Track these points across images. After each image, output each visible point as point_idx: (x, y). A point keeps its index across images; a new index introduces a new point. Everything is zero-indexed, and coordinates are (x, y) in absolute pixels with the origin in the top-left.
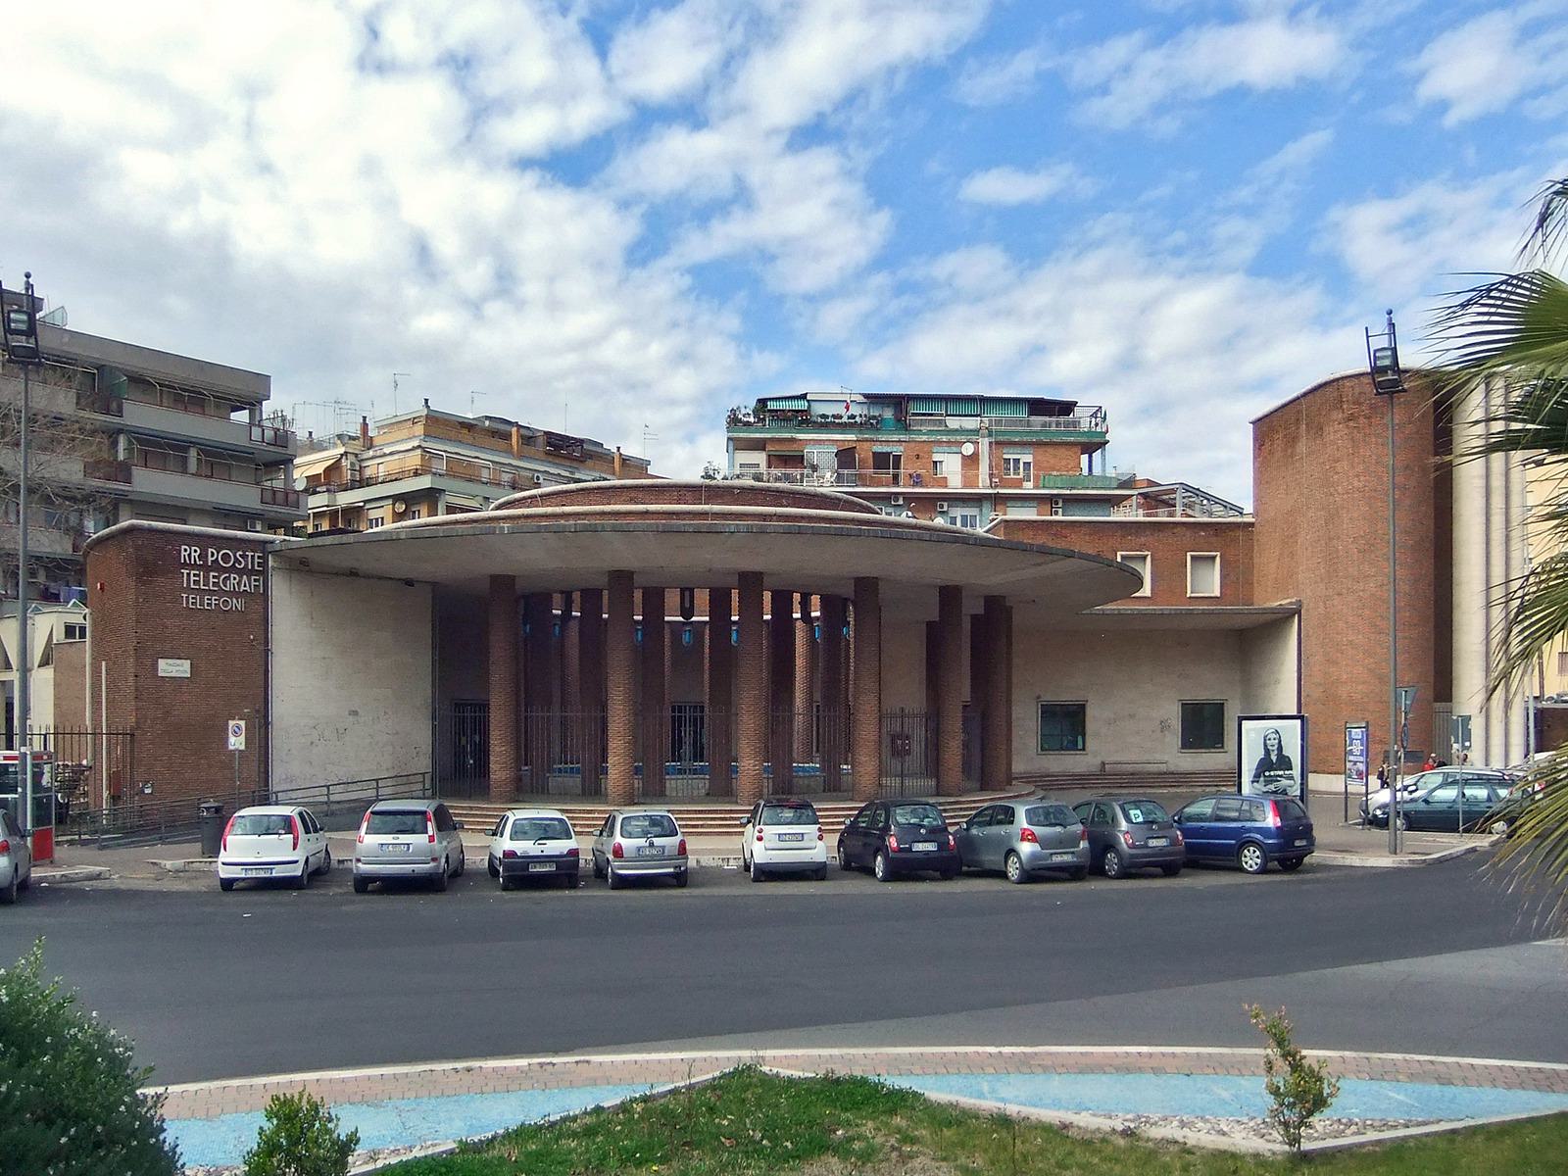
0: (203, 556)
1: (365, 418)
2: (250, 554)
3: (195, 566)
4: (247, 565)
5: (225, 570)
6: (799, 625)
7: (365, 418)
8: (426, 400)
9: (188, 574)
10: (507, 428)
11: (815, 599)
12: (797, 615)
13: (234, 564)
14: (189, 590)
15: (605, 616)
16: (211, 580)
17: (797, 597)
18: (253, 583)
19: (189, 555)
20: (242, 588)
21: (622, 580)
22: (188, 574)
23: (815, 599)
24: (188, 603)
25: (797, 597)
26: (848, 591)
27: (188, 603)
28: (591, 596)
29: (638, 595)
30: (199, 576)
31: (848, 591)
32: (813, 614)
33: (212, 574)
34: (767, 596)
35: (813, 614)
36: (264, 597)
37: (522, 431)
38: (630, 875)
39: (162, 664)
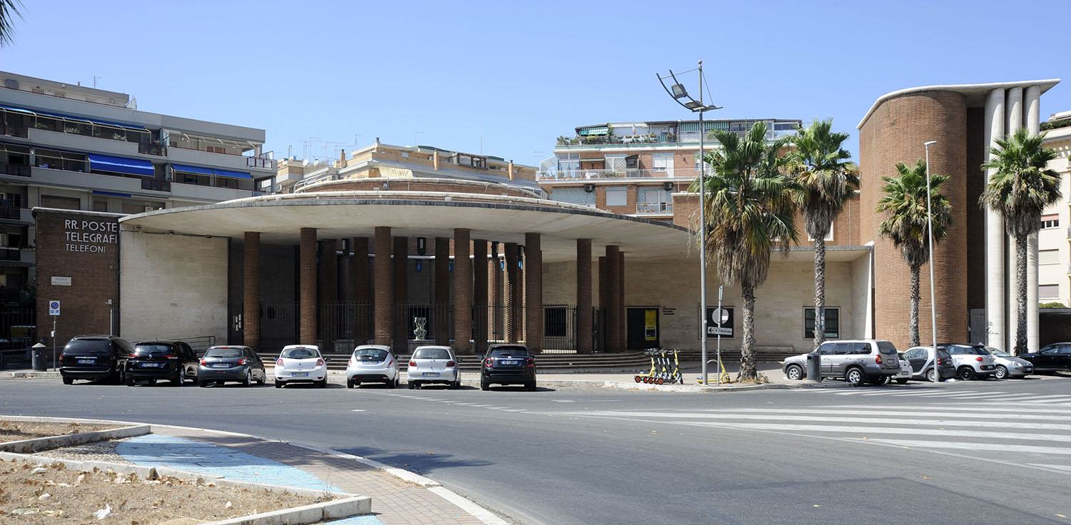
0: (79, 225)
1: (343, 150)
2: (109, 224)
3: (74, 230)
4: (107, 229)
5: (92, 232)
6: (490, 264)
7: (343, 150)
8: (378, 139)
9: (70, 234)
10: (429, 152)
11: (501, 246)
12: (490, 256)
13: (98, 229)
14: (70, 242)
15: (452, 257)
16: (84, 237)
17: (490, 244)
18: (111, 238)
19: (71, 225)
20: (104, 241)
21: (462, 235)
22: (70, 234)
23: (501, 246)
24: (69, 249)
25: (490, 244)
26: (522, 241)
27: (69, 249)
28: (442, 243)
29: (472, 243)
30: (76, 235)
31: (522, 241)
32: (450, 257)
33: (85, 234)
34: (472, 243)
35: (499, 255)
36: (118, 246)
37: (441, 153)
38: (607, 409)
39: (53, 279)
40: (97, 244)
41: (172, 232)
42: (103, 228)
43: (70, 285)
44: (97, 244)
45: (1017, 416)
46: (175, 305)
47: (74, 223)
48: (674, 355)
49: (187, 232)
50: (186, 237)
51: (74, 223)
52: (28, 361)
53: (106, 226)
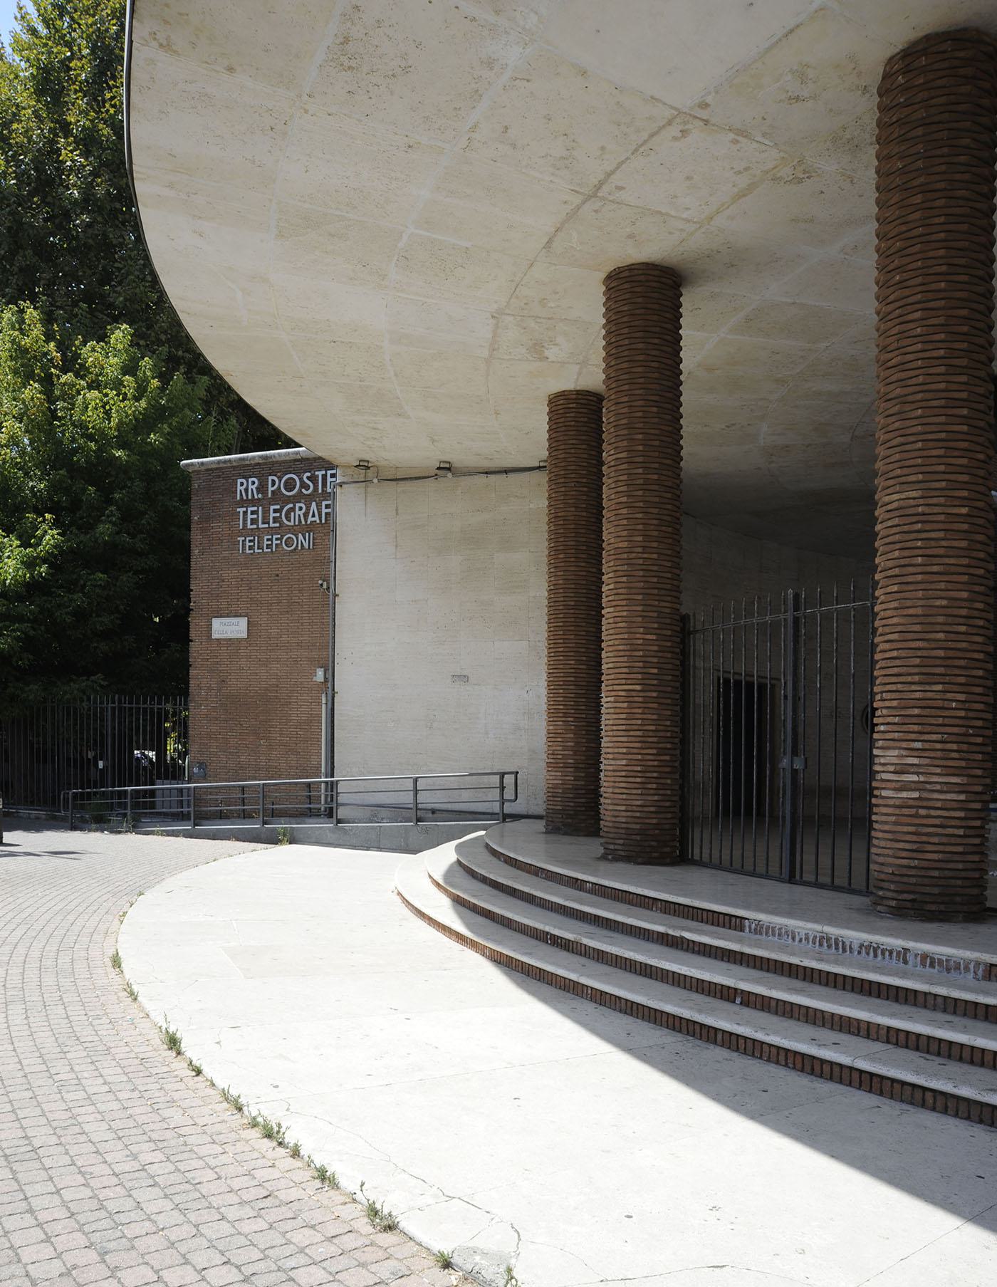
3: (253, 502)
4: (316, 489)
9: (245, 513)
18: (324, 511)
19: (246, 490)
20: (310, 519)
33: (272, 508)
40: (294, 530)
41: (446, 468)
42: (307, 488)
43: (215, 636)
44: (294, 530)
45: (567, 931)
46: (464, 678)
47: (253, 484)
48: (326, 783)
49: (408, 483)
50: (492, 477)
51: (253, 484)
52: (684, 840)
53: (313, 479)
